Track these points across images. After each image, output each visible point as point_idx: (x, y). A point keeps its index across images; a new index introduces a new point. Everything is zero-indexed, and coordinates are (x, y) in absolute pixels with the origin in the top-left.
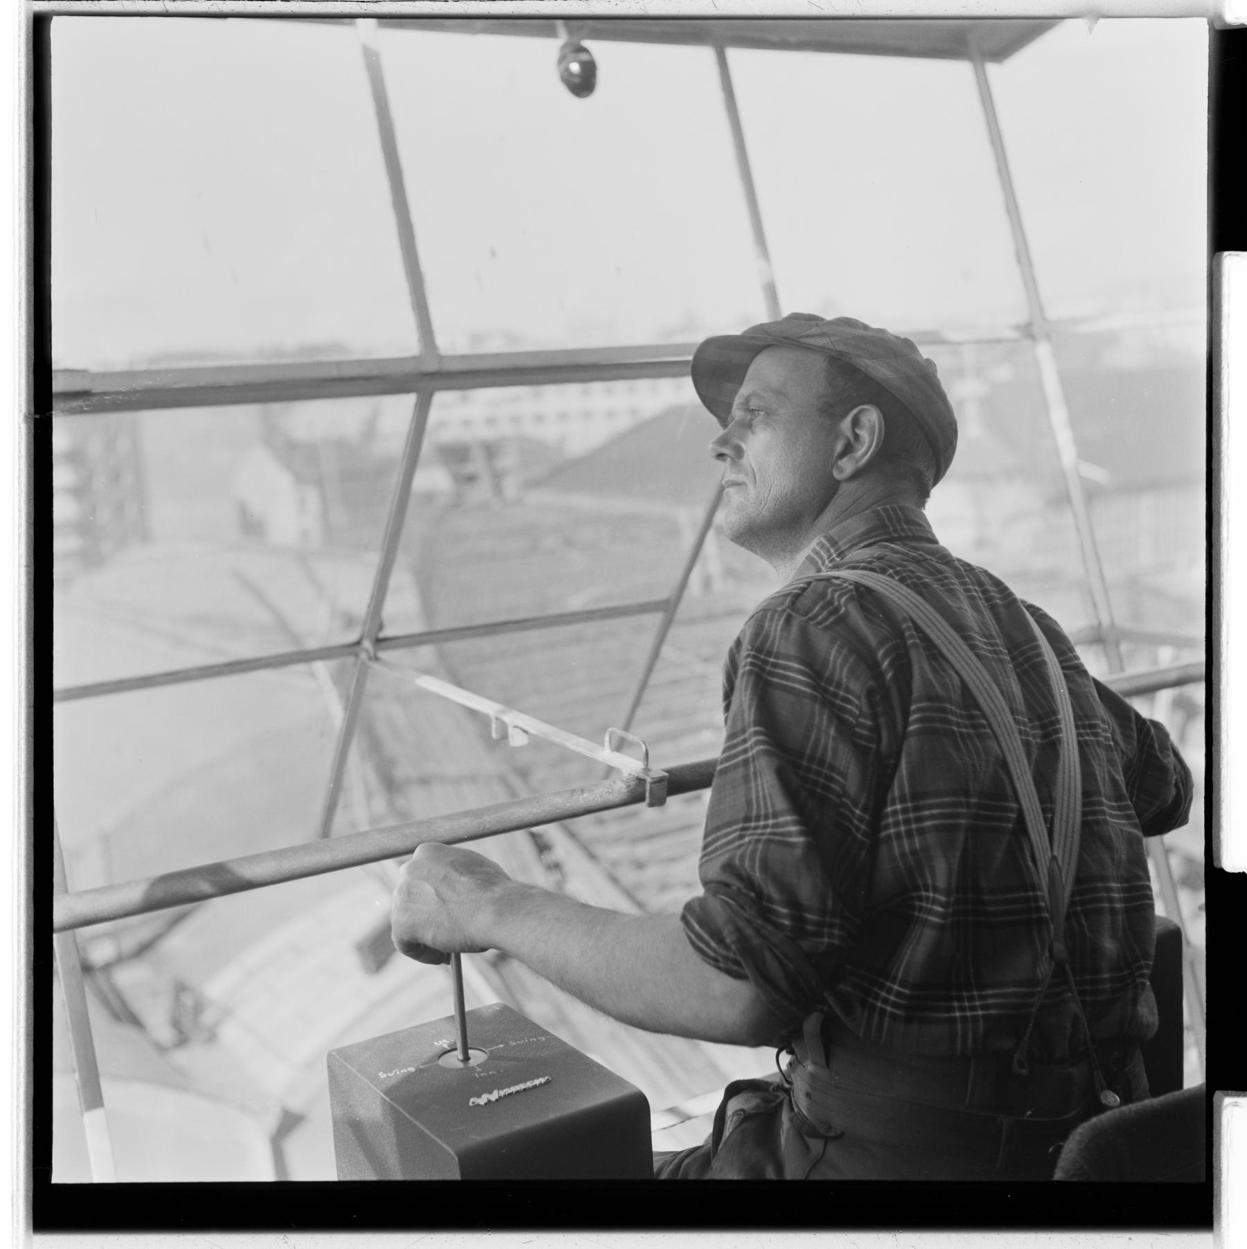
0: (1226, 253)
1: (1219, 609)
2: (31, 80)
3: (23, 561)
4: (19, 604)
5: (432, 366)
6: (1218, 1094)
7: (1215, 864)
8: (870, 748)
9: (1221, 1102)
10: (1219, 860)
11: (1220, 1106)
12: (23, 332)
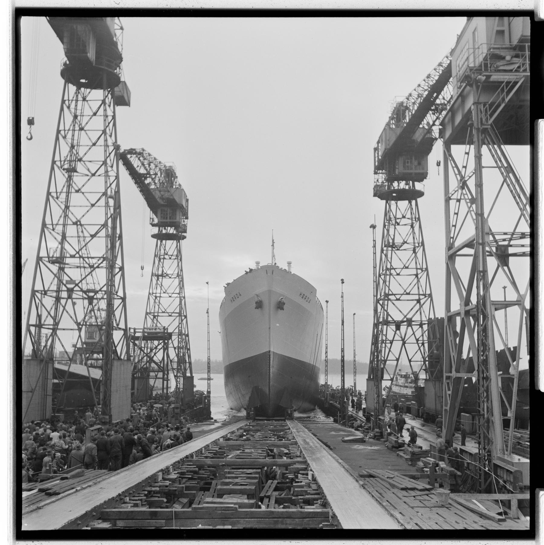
0: (540, 120)
4: (10, 275)
6: (537, 489)
7: (536, 389)
9: (539, 493)
10: (538, 386)
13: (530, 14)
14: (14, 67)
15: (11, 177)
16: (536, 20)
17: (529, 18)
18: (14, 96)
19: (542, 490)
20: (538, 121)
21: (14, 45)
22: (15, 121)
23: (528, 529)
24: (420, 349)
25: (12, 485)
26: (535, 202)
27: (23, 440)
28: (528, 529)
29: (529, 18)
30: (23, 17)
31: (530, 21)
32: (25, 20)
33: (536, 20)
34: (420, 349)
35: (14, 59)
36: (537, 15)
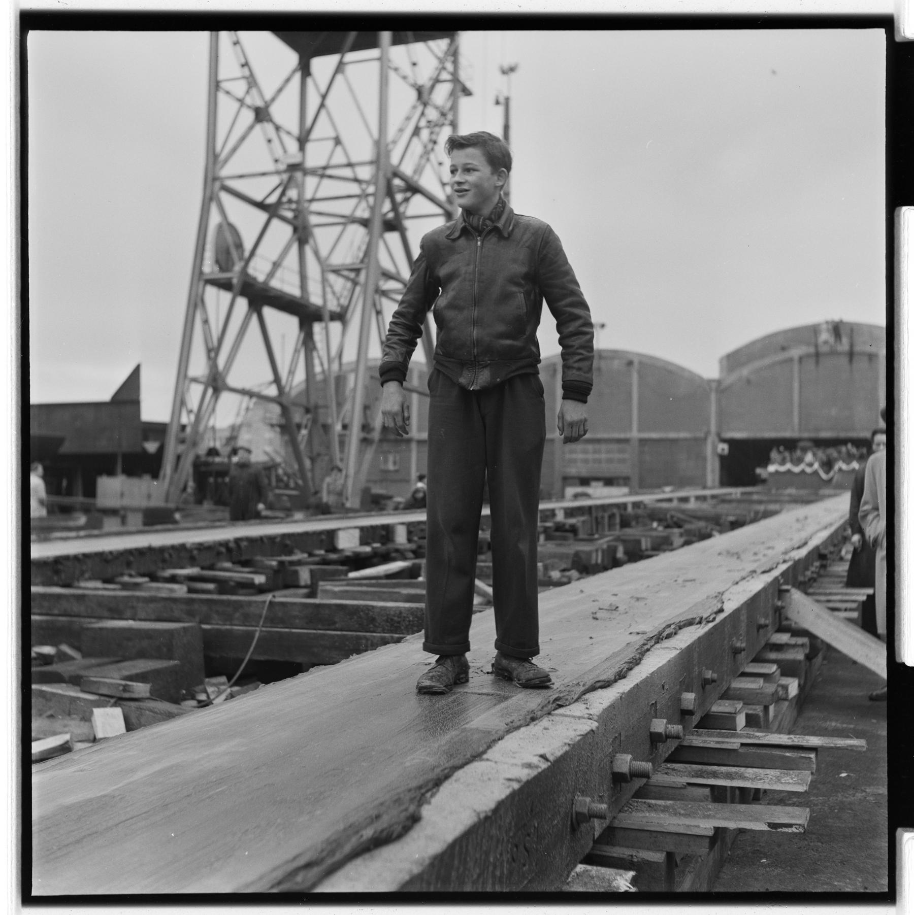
0: (904, 208)
1: (899, 320)
2: (19, 281)
3: (14, 574)
5: (304, 36)
6: (899, 830)
7: (898, 660)
8: (630, 428)
9: (902, 836)
10: (900, 656)
11: (901, 839)
12: (14, 553)
13: (886, 23)
14: (19, 119)
15: (14, 304)
16: (898, 39)
17: (883, 30)
18: (19, 168)
19: (907, 831)
20: (900, 211)
21: (19, 81)
22: (19, 209)
23: (887, 890)
24: (350, 165)
25: (14, 828)
26: (896, 346)
27: (437, 890)
28: (887, 890)
29: (883, 30)
30: (30, 32)
31: (885, 36)
32: (33, 36)
33: (898, 39)
34: (350, 165)
35: (19, 106)
36: (899, 32)
